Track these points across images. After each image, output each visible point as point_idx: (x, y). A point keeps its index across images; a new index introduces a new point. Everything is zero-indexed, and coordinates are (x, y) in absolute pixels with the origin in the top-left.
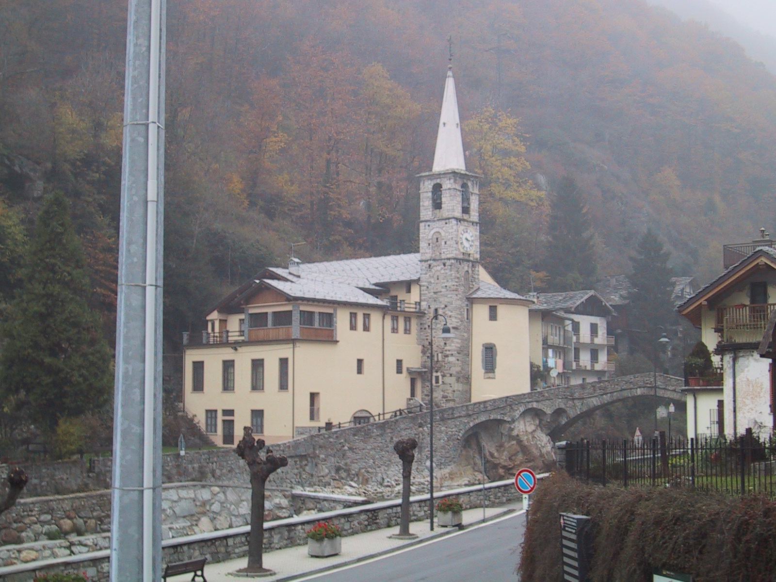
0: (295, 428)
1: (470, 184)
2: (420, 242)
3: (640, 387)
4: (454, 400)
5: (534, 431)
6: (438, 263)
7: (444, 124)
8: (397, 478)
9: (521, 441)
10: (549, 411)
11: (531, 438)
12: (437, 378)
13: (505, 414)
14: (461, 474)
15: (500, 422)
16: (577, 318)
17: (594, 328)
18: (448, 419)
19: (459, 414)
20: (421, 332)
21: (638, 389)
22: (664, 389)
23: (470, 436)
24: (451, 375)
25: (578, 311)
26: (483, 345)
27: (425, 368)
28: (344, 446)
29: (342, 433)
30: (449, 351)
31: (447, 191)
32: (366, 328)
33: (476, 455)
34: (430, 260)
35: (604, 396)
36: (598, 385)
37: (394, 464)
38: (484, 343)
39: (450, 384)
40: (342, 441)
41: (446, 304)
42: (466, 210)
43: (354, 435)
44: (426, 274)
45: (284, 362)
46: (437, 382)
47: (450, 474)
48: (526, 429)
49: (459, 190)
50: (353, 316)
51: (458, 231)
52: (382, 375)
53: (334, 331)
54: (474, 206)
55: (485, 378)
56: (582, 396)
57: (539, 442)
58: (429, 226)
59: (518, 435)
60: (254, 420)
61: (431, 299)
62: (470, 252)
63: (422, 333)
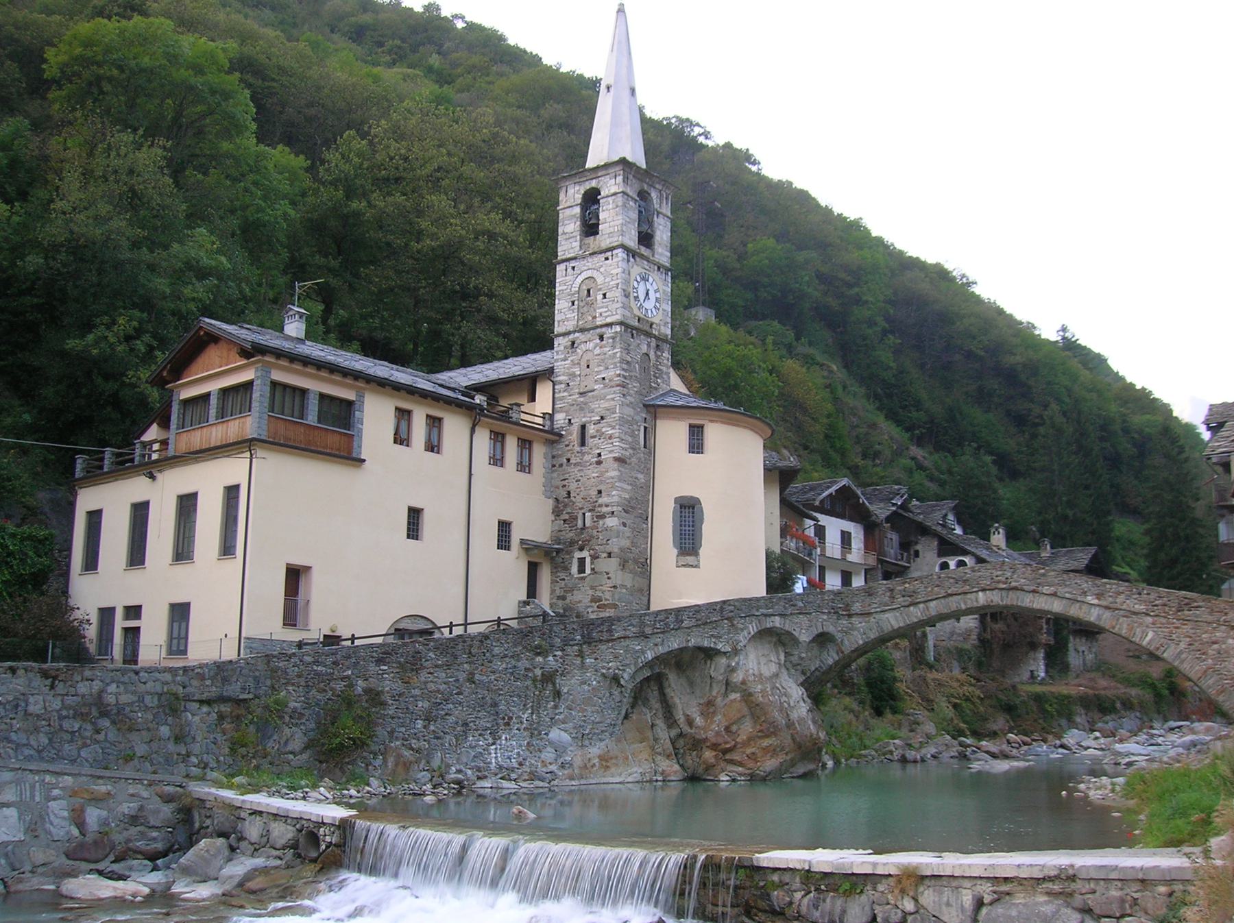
1: (654, 195)
2: (557, 301)
3: (983, 590)
4: (615, 606)
5: (776, 675)
6: (589, 335)
7: (608, 88)
9: (750, 694)
12: (582, 561)
13: (718, 637)
14: (627, 758)
15: (709, 654)
16: (824, 519)
17: (846, 538)
18: (601, 641)
19: (621, 634)
20: (553, 472)
21: (980, 593)
22: (1034, 591)
24: (609, 555)
26: (677, 500)
27: (559, 544)
30: (607, 506)
31: (610, 199)
32: (433, 447)
33: (658, 722)
34: (574, 332)
35: (912, 608)
36: (899, 588)
37: (476, 734)
39: (608, 574)
42: (646, 239)
43: (380, 661)
44: (565, 359)
46: (582, 569)
49: (632, 198)
50: (403, 415)
53: (355, 438)
56: (867, 609)
60: (176, 625)
61: (575, 407)
62: (654, 320)
63: (555, 475)
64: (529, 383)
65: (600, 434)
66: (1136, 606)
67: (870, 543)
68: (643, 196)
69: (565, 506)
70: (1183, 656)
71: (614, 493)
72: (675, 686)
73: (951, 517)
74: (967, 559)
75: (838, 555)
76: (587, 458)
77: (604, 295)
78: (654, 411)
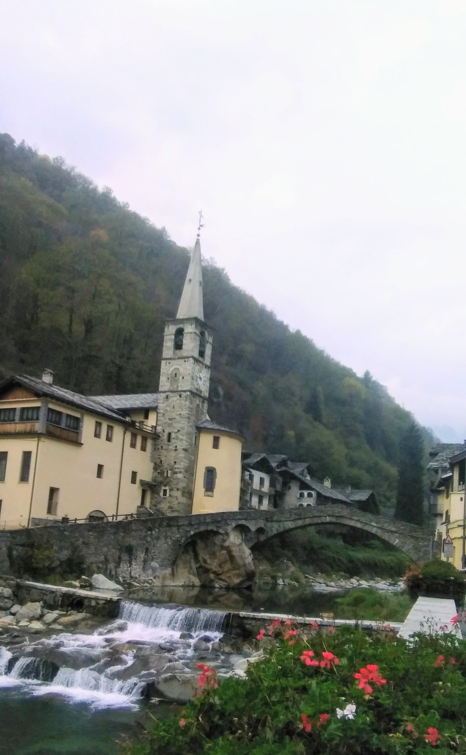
5: (240, 544)
7: (190, 280)
8: (124, 575)
10: (253, 529)
11: (238, 550)
12: (165, 491)
17: (262, 480)
19: (182, 523)
28: (78, 540)
29: (76, 527)
30: (178, 469)
31: (189, 335)
32: (109, 439)
34: (168, 391)
38: (207, 466)
39: (177, 497)
40: (77, 535)
41: (179, 429)
42: (202, 354)
43: (89, 531)
44: (163, 403)
45: (27, 456)
46: (165, 494)
50: (98, 425)
52: (118, 481)
55: (205, 496)
58: (169, 363)
63: (155, 453)
64: (146, 412)
65: (177, 438)
66: (393, 529)
67: (272, 484)
68: (202, 334)
69: (159, 466)
70: (410, 551)
72: (200, 545)
73: (306, 471)
74: (313, 492)
75: (258, 489)
76: (170, 447)
77: (183, 378)
78: (200, 430)
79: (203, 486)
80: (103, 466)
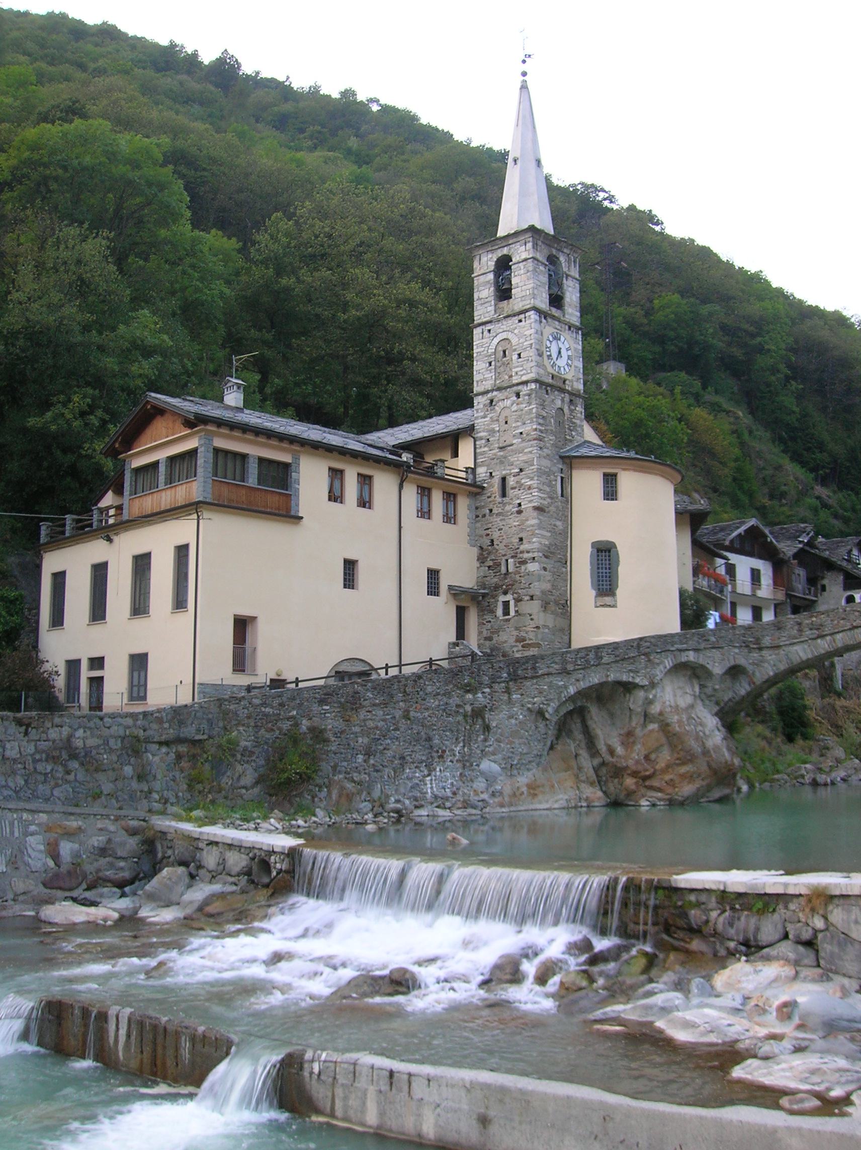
0: (196, 686)
1: (562, 259)
2: (475, 363)
4: (538, 645)
5: (692, 706)
6: (505, 393)
7: (515, 161)
9: (668, 725)
10: (718, 670)
12: (506, 604)
13: (636, 672)
14: (553, 786)
15: (628, 687)
16: (734, 558)
17: (755, 575)
19: (545, 670)
20: (477, 522)
23: (570, 713)
24: (532, 598)
25: (732, 549)
26: (594, 544)
30: (528, 552)
32: (365, 502)
33: (581, 752)
34: (492, 391)
35: (819, 641)
37: (413, 766)
41: (522, 465)
42: (556, 300)
43: (322, 702)
44: (485, 417)
45: (182, 551)
46: (506, 612)
47: (530, 786)
48: (675, 702)
49: (543, 264)
50: (336, 474)
51: (542, 334)
54: (571, 299)
55: (596, 607)
56: (776, 643)
57: (699, 728)
58: (489, 331)
59: (661, 714)
60: (136, 674)
62: (566, 377)
63: (478, 525)
64: (452, 440)
65: (520, 486)
67: (779, 579)
68: (552, 260)
71: (534, 540)
72: (597, 718)
77: (519, 355)
78: (569, 462)
79: (590, 584)
80: (357, 561)
